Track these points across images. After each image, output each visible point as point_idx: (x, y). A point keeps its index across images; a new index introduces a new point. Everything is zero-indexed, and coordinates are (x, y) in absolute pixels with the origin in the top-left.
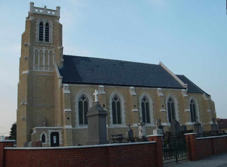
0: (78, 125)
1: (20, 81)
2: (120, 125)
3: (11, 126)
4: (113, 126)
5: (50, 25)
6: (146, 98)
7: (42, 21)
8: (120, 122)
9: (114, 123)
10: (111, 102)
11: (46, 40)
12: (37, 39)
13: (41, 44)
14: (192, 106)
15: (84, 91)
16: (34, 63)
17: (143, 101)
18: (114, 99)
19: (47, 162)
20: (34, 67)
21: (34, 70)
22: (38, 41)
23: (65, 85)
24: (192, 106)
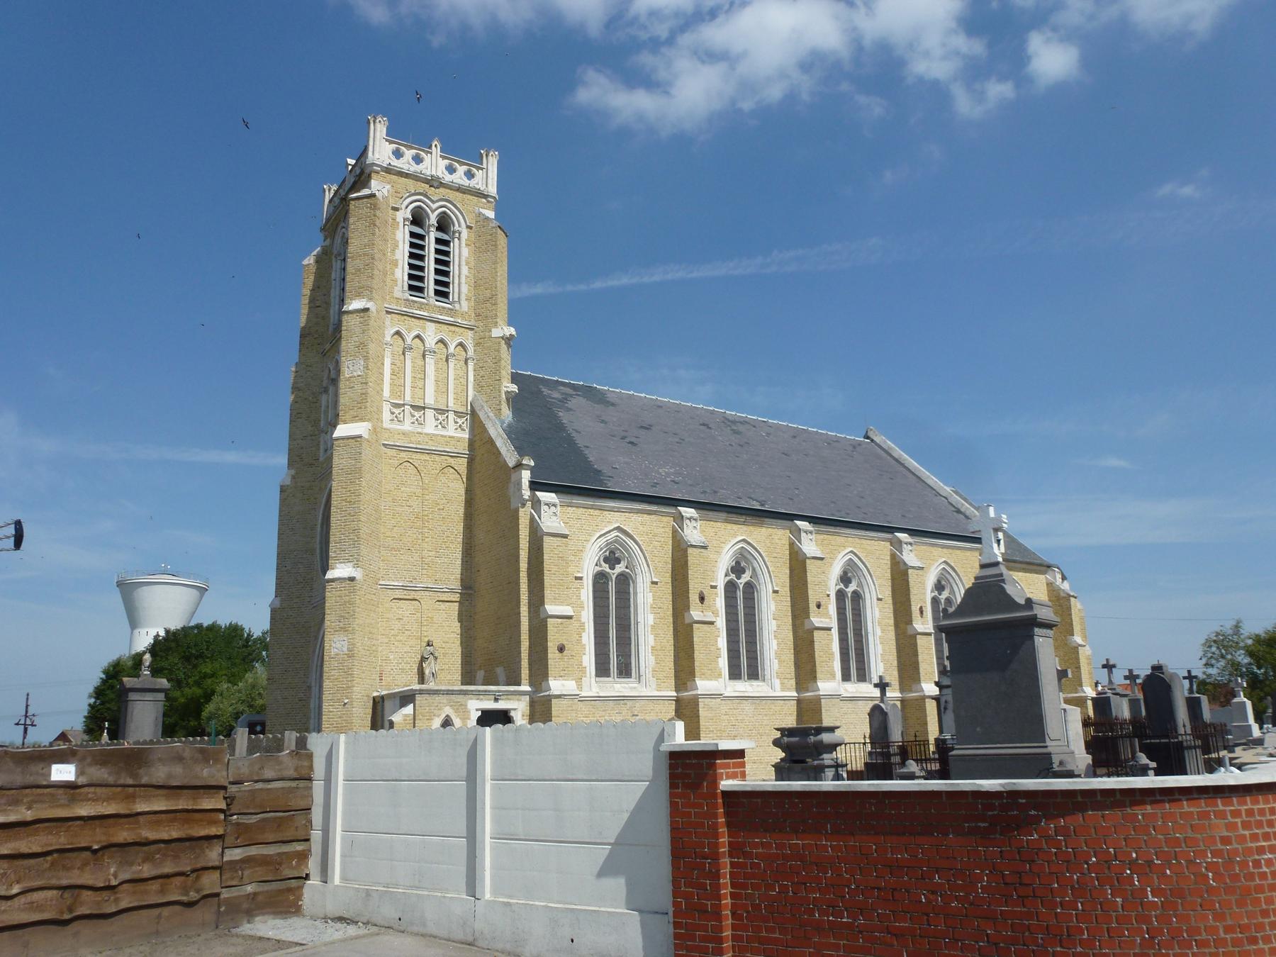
0: (593, 679)
1: (293, 472)
2: (755, 683)
3: (95, 677)
4: (593, 686)
5: (457, 228)
6: (743, 564)
7: (444, 213)
8: (754, 675)
9: (735, 674)
10: (721, 582)
11: (437, 293)
12: (400, 283)
13: (420, 309)
14: (740, 594)
15: (744, 540)
16: (386, 393)
17: (733, 576)
18: (606, 560)
19: (1150, 863)
20: (386, 408)
21: (387, 424)
22: (407, 295)
23: (544, 496)
24: (740, 594)
